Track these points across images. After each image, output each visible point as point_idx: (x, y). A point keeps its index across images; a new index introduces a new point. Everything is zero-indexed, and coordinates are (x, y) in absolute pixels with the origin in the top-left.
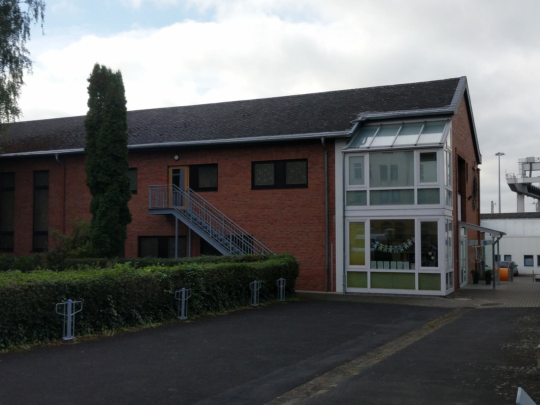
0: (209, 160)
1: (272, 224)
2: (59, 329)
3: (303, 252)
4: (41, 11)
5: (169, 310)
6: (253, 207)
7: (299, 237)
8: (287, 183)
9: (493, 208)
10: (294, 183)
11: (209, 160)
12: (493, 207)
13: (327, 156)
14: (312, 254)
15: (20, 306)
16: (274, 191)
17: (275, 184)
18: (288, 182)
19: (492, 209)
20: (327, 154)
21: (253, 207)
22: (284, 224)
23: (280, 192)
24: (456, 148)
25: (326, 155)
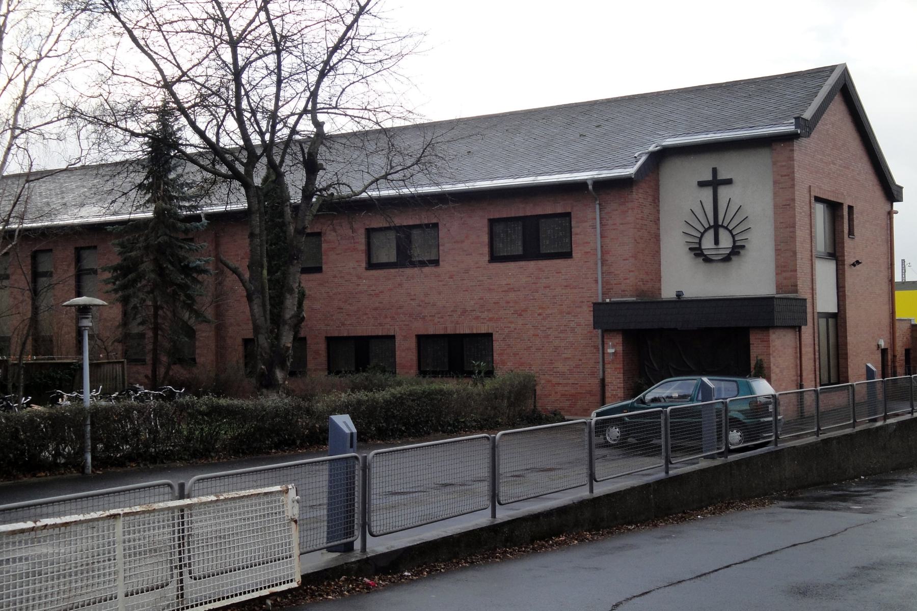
0: (424, 218)
1: (521, 315)
2: (153, 450)
3: (566, 358)
4: (121, 513)
5: (197, 438)
6: (785, 176)
7: (561, 335)
8: (542, 252)
9: (905, 272)
10: (552, 251)
11: (424, 218)
12: (905, 270)
13: (600, 209)
14: (580, 360)
15: (134, 403)
16: (522, 263)
17: (524, 250)
18: (544, 250)
19: (902, 275)
20: (600, 204)
21: (785, 176)
22: (538, 315)
23: (531, 265)
24: (810, 186)
25: (598, 206)
